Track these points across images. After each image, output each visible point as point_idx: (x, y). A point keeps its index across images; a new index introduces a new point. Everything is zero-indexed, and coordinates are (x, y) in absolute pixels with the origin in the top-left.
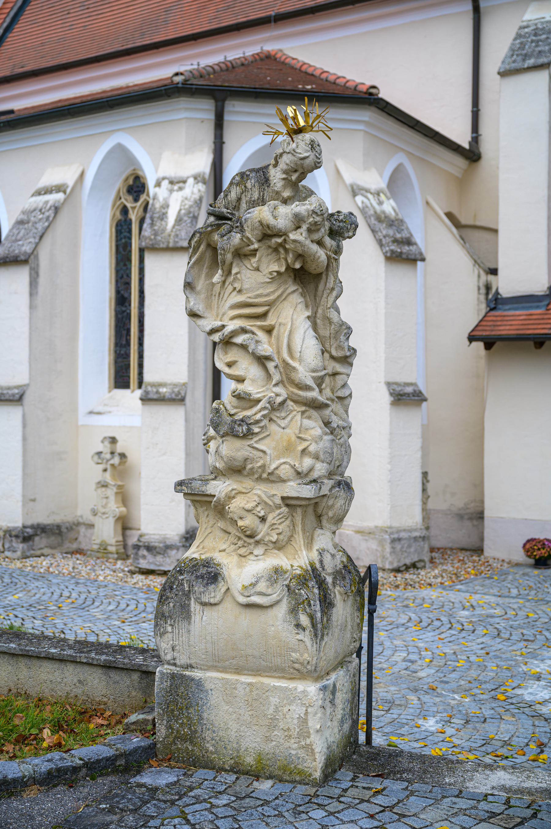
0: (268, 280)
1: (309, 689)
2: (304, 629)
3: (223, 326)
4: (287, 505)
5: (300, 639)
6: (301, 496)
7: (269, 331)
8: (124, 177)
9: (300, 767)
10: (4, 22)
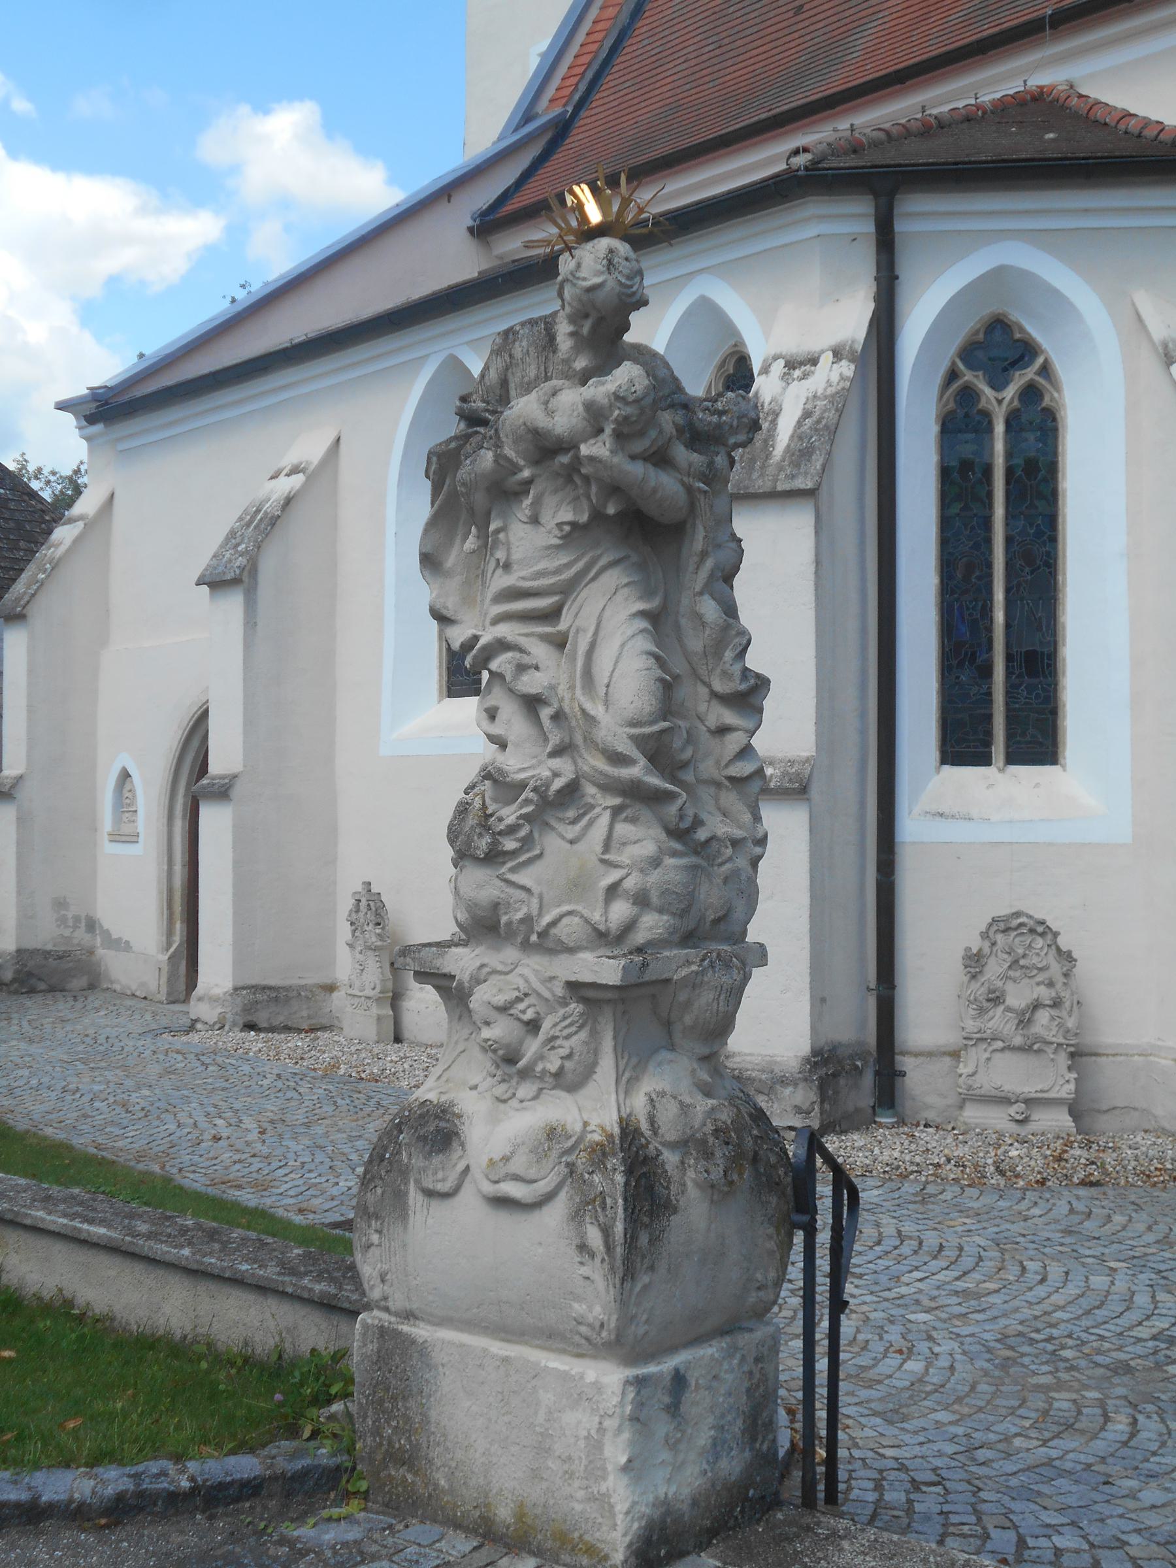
0: (557, 541)
1: (606, 1380)
2: (592, 1255)
3: (476, 638)
4: (584, 1000)
5: (585, 1274)
6: (599, 981)
7: (560, 643)
8: (716, 360)
9: (587, 1538)
10: (576, 89)
